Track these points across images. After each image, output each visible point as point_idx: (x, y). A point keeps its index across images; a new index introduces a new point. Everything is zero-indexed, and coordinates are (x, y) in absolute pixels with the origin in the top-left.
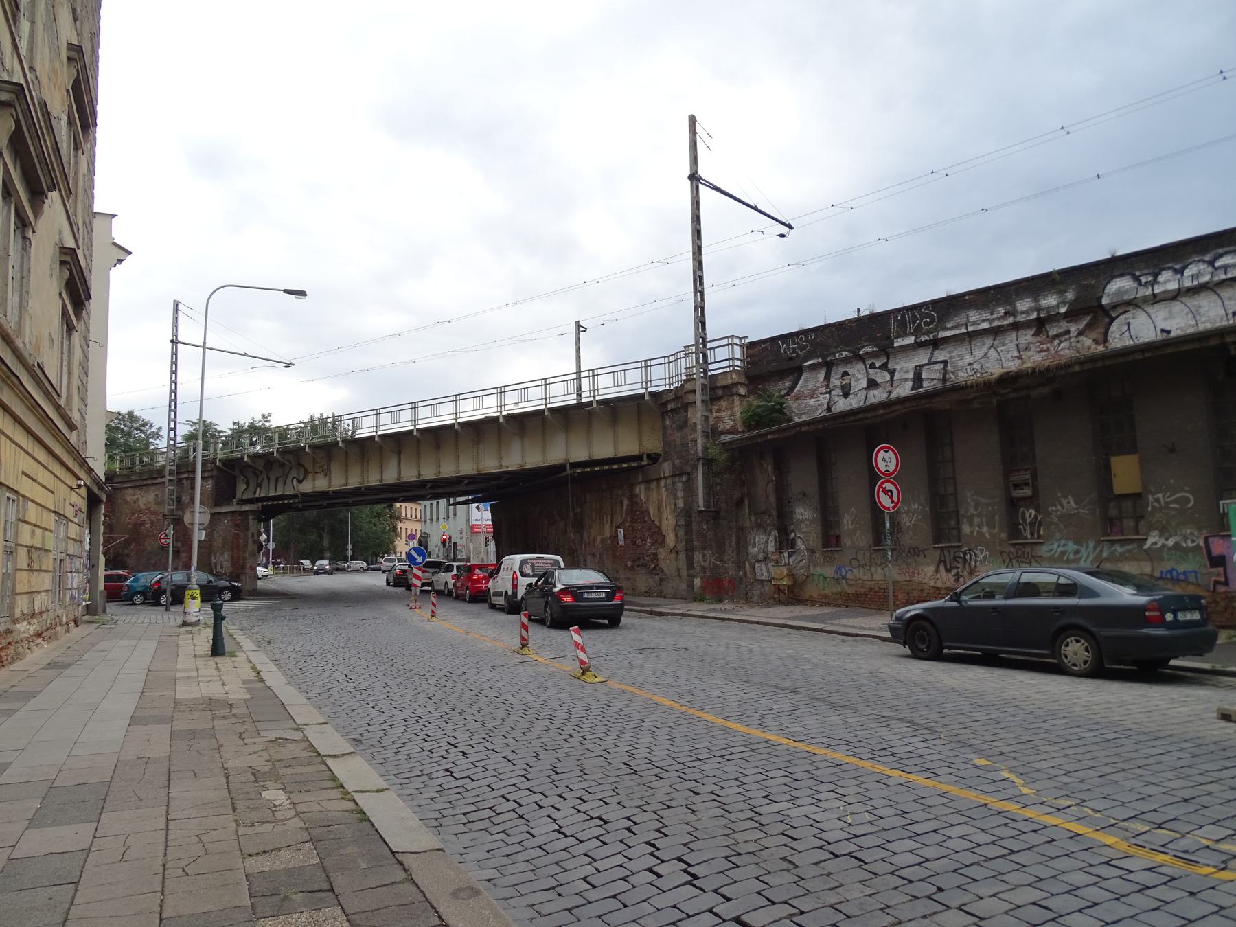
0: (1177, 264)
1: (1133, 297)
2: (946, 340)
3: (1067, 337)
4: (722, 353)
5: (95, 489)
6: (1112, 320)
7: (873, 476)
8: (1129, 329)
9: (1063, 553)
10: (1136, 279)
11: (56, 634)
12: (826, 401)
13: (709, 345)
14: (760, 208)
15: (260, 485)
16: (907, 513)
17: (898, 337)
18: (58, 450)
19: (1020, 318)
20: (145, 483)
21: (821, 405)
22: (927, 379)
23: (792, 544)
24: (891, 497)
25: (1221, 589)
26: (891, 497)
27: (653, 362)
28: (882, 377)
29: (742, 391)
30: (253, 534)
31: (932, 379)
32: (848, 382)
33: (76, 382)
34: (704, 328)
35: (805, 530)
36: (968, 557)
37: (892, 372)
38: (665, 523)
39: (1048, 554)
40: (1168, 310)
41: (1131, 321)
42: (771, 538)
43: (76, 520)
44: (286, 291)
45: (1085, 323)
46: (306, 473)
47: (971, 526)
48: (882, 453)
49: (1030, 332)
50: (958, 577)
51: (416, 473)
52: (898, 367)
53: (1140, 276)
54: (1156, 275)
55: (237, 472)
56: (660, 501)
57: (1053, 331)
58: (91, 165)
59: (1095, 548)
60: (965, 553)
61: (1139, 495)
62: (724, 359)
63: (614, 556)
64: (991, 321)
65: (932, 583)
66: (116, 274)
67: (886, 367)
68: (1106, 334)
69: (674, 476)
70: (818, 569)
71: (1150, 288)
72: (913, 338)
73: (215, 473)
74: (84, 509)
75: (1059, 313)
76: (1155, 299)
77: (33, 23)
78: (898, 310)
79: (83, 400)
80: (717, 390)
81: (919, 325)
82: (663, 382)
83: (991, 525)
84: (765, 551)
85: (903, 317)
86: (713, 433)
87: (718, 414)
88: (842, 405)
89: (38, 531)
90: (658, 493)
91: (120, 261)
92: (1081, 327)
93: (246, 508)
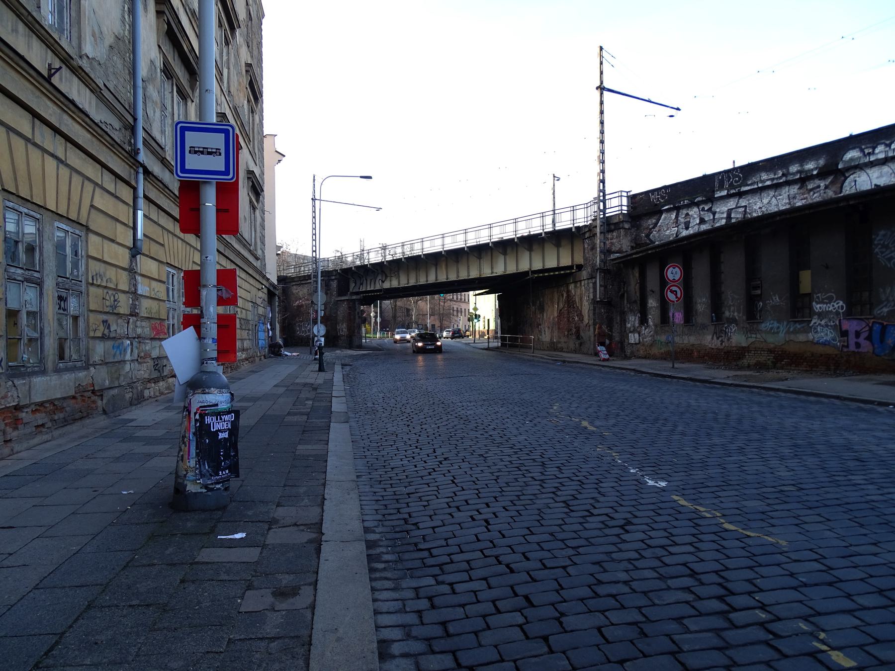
0: (888, 140)
1: (857, 163)
2: (746, 192)
3: (818, 189)
4: (615, 202)
5: (272, 289)
6: (846, 178)
7: (664, 282)
8: (855, 184)
9: (772, 328)
10: (862, 151)
11: (255, 361)
12: (675, 232)
13: (607, 197)
14: (652, 101)
15: (362, 284)
16: (700, 303)
17: (717, 191)
18: (251, 271)
19: (790, 178)
20: (302, 282)
21: (673, 234)
22: (734, 218)
23: (647, 322)
24: (676, 295)
25: (845, 350)
26: (676, 295)
27: (578, 207)
28: (708, 217)
29: (627, 226)
30: (358, 313)
31: (737, 216)
32: (689, 220)
33: (258, 235)
34: (604, 187)
35: (653, 313)
36: (727, 330)
37: (714, 214)
38: (584, 308)
39: (764, 329)
40: (880, 171)
41: (857, 179)
42: (637, 318)
43: (262, 305)
44: (361, 177)
45: (830, 180)
46: (386, 277)
47: (729, 312)
48: (671, 269)
49: (797, 187)
50: (722, 342)
51: (425, 280)
52: (718, 210)
53: (864, 149)
54: (874, 148)
55: (349, 277)
56: (581, 294)
57: (810, 186)
58: (261, 117)
59: (787, 326)
60: (726, 328)
61: (810, 294)
62: (616, 206)
63: (559, 328)
64: (772, 179)
65: (710, 346)
66: (278, 168)
67: (711, 210)
68: (841, 187)
69: (588, 279)
70: (659, 337)
71: (868, 158)
72: (726, 191)
73: (338, 277)
74: (266, 300)
75: (812, 175)
76: (872, 164)
77: (229, 69)
78: (720, 173)
79: (263, 243)
80: (609, 224)
81: (732, 182)
82: (583, 220)
83: (739, 312)
84: (634, 326)
85: (723, 177)
86: (607, 252)
87: (612, 241)
88: (685, 233)
89: (244, 311)
90: (580, 289)
91: (280, 161)
92: (827, 183)
93: (354, 297)
